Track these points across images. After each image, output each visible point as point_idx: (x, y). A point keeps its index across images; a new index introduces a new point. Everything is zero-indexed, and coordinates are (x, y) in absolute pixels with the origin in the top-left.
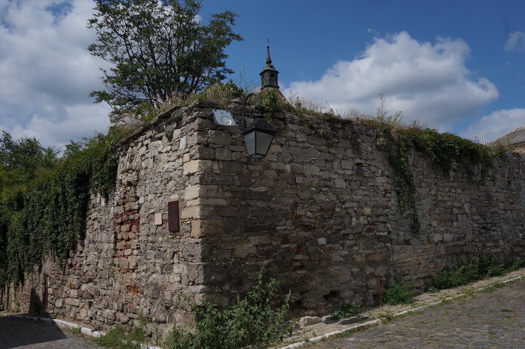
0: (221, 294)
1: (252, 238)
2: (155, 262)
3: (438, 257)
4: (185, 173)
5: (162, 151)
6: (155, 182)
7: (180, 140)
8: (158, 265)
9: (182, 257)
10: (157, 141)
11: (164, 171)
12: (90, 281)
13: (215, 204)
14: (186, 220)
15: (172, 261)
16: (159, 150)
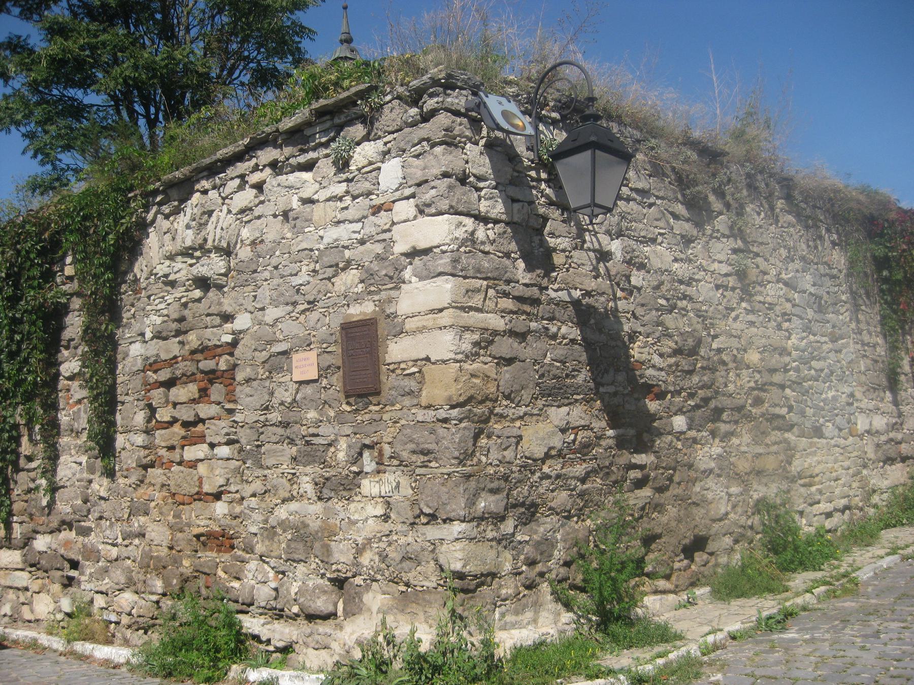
0: (499, 542)
1: (552, 411)
2: (294, 474)
3: (865, 466)
4: (400, 248)
5: (316, 197)
6: (291, 275)
7: (379, 169)
8: (307, 479)
9: (391, 457)
10: (297, 174)
11: (322, 247)
12: (67, 524)
13: (483, 325)
14: (403, 366)
15: (354, 469)
16: (305, 195)
